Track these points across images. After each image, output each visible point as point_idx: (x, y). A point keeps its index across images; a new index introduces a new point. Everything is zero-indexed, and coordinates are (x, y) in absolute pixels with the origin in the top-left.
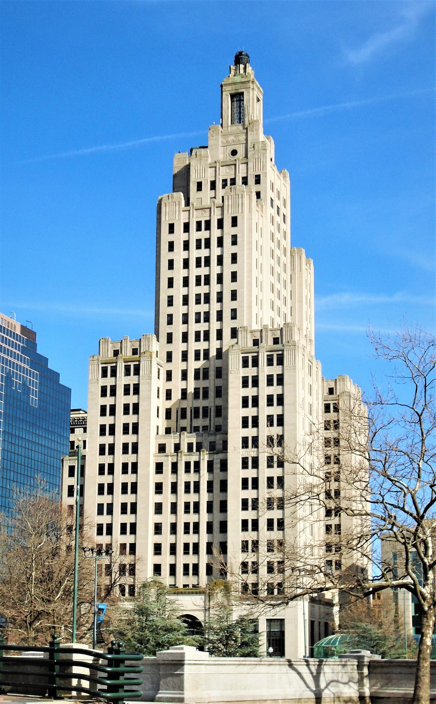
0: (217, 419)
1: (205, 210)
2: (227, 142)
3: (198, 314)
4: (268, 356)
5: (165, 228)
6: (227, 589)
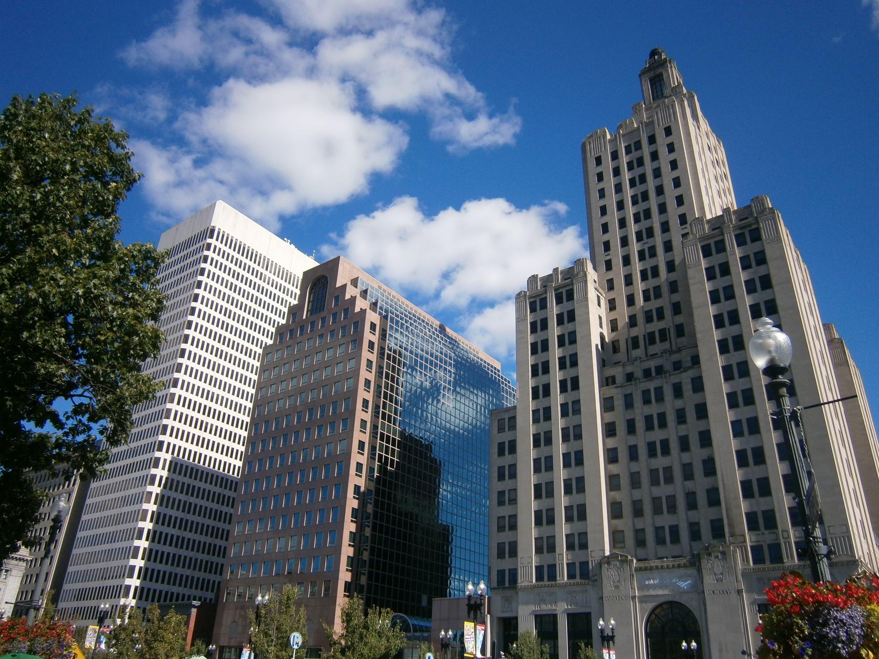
0: (679, 340)
5: (592, 163)
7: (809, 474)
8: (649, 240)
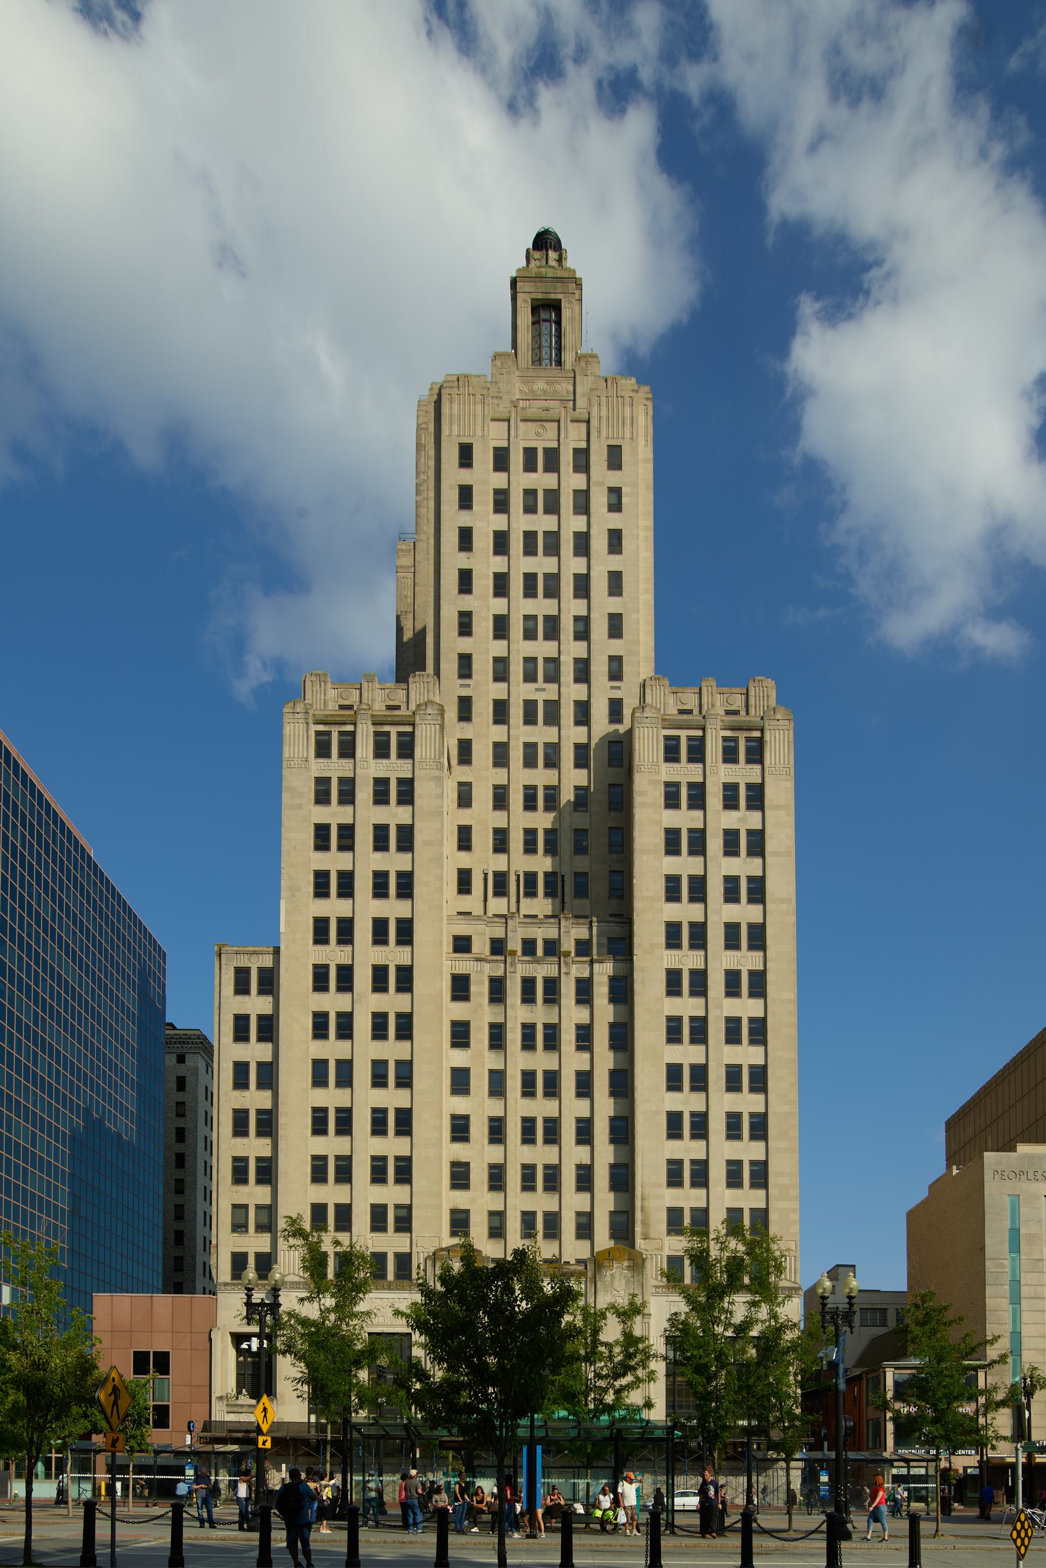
0: (577, 901)
1: (545, 424)
2: (532, 391)
3: (530, 662)
4: (725, 739)
5: (451, 455)
6: (637, 1264)
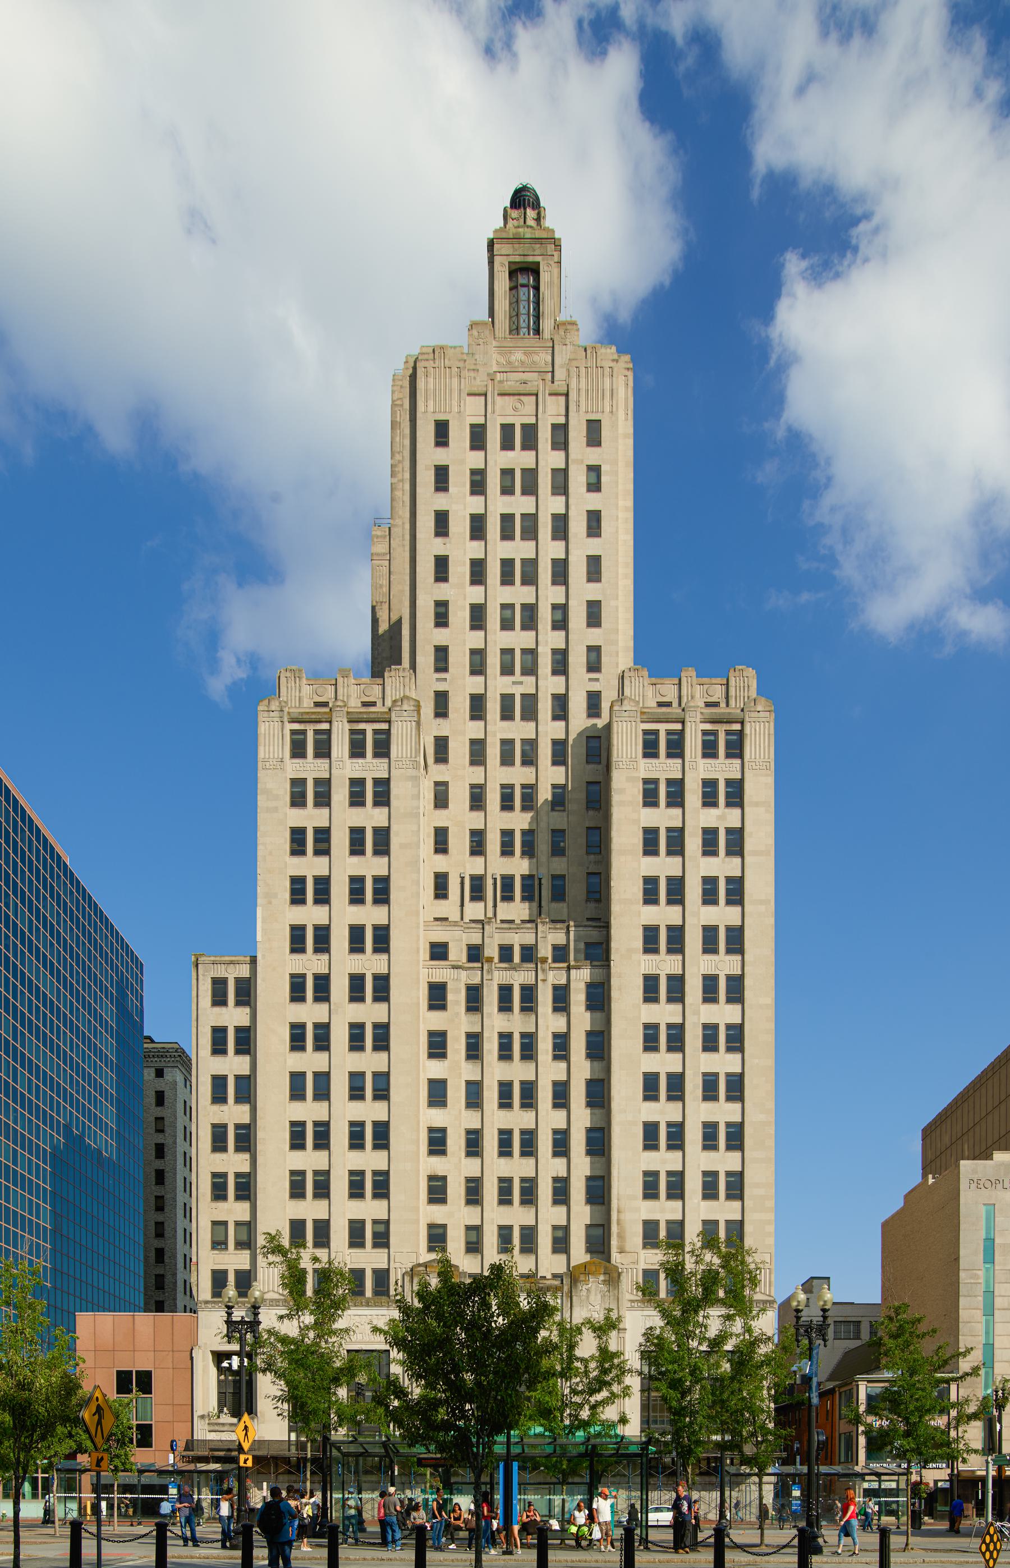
0: (554, 905)
1: (522, 398)
5: (426, 433)
6: (613, 1278)
7: (990, 1295)
8: (524, 679)
